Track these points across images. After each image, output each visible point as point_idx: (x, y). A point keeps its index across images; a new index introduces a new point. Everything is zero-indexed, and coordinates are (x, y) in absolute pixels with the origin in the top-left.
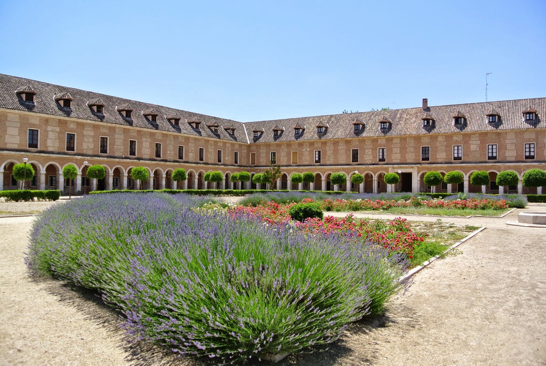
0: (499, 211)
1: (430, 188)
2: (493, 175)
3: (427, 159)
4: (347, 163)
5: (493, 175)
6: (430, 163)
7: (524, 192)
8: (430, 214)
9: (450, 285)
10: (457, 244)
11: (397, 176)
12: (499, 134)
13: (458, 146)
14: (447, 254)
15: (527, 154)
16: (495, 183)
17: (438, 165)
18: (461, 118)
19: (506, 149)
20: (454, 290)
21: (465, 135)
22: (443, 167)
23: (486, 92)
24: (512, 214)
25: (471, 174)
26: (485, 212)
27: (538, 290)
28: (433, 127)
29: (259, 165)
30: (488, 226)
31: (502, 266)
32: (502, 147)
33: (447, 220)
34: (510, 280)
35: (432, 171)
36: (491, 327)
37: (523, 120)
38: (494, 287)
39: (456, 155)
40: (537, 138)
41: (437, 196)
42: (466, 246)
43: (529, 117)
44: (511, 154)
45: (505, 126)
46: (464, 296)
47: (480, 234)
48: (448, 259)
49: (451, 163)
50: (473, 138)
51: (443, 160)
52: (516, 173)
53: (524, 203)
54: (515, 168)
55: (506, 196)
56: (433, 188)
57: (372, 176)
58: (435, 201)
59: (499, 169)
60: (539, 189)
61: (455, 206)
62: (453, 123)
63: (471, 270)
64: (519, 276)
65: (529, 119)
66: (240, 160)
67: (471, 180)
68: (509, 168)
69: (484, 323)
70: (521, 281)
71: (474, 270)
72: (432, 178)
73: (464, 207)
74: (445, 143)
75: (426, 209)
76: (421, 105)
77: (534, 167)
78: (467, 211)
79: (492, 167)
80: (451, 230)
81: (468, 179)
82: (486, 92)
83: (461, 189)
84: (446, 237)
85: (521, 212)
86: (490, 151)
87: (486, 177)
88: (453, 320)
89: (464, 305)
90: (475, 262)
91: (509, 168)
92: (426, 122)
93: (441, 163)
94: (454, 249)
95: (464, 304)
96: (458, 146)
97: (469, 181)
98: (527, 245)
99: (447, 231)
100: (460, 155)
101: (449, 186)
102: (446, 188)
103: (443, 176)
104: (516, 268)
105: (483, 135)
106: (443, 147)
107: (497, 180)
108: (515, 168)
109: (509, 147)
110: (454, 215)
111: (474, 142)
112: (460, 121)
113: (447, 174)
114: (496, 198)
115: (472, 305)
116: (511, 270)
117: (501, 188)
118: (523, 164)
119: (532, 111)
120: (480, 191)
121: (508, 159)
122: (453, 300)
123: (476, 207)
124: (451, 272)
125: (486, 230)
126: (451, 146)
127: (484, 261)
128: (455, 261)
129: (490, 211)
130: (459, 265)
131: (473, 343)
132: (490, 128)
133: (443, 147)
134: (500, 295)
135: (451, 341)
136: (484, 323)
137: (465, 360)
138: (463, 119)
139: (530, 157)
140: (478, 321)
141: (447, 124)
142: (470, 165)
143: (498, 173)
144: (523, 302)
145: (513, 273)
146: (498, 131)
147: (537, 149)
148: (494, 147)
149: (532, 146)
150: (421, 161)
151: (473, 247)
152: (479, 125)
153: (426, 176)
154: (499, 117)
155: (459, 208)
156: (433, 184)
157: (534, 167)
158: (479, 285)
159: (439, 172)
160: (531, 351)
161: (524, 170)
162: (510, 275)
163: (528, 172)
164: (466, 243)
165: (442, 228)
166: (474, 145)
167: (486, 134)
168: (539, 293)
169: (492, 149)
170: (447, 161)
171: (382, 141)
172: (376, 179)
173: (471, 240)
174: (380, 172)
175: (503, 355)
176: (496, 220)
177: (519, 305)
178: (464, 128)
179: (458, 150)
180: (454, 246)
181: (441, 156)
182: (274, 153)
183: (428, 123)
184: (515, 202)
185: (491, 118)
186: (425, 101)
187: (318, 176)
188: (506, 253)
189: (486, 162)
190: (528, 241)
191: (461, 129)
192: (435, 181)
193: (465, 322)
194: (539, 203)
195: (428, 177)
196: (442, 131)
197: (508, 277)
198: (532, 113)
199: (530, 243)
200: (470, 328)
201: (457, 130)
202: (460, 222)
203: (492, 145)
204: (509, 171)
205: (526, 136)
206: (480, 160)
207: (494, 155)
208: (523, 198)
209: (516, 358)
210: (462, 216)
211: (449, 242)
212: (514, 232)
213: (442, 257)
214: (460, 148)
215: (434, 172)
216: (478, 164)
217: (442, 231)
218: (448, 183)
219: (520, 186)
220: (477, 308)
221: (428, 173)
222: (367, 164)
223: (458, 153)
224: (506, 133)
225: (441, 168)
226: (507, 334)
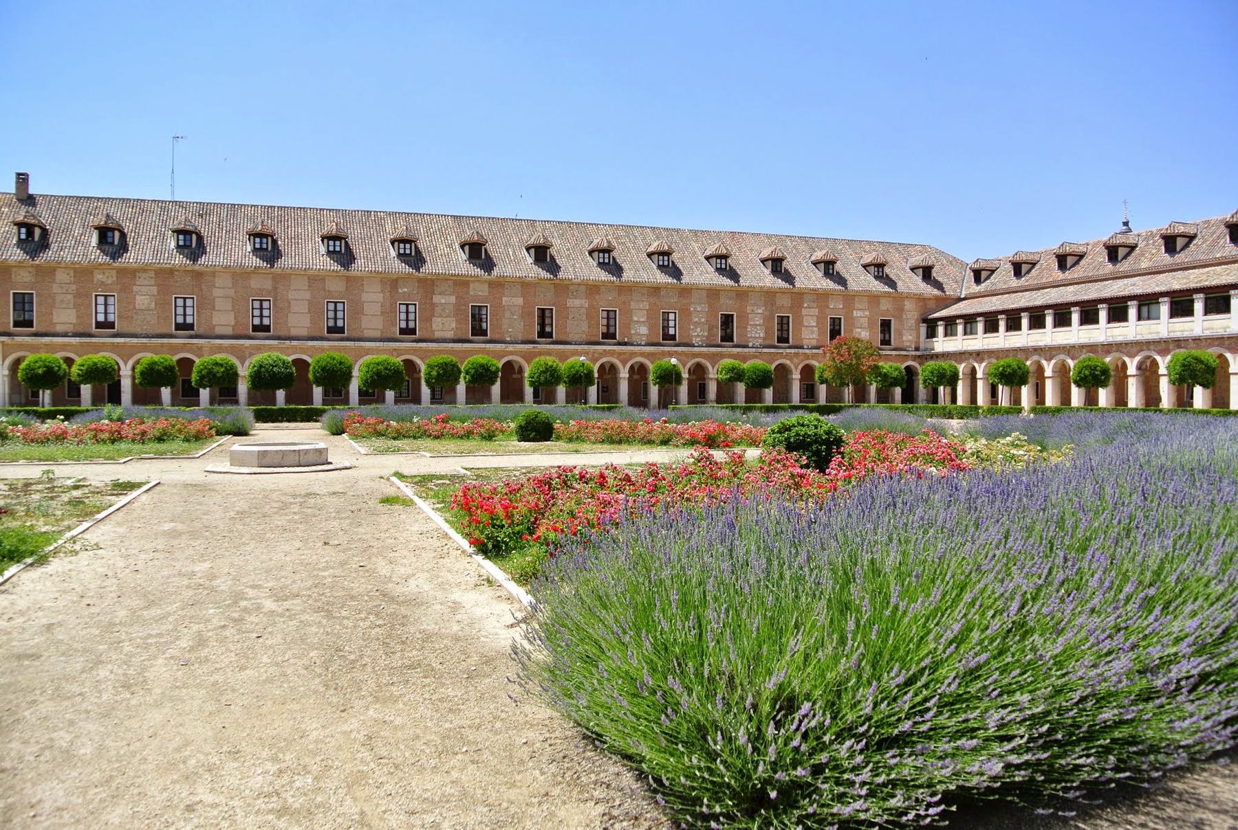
0: (193, 445)
1: (36, 395)
2: (186, 364)
4: (460, 336)
5: (186, 364)
6: (36, 335)
7: (252, 400)
8: (30, 459)
9: (49, 627)
10: (85, 525)
12: (198, 275)
13: (106, 296)
14: (56, 552)
15: (257, 321)
16: (189, 381)
17: (56, 339)
18: (113, 230)
19: (214, 309)
20: (60, 634)
21: (122, 272)
23: (172, 178)
24: (220, 449)
25: (138, 362)
26: (162, 447)
27: (243, 603)
28: (44, 244)
29: (52, 330)
30: (165, 478)
31: (178, 565)
32: (206, 304)
33: (67, 472)
34: (191, 593)
35: (271, 353)
36: (134, 702)
37: (249, 248)
38: (155, 612)
39: (101, 318)
40: (275, 288)
41: (52, 415)
42: (104, 528)
43: (261, 243)
44: (223, 320)
45: (210, 259)
46: (78, 646)
47: (144, 497)
48: (55, 565)
49: (90, 335)
50: (142, 279)
51: (69, 328)
52: (234, 361)
53: (247, 426)
54: (232, 350)
55: (212, 411)
56: (46, 396)
57: (521, 370)
58: (48, 426)
59: (199, 351)
60: (281, 394)
61: (95, 436)
62: (94, 240)
63: (108, 582)
64: (211, 580)
65: (261, 249)
67: (137, 375)
68: (220, 349)
69: (118, 698)
70: (213, 589)
71: (114, 580)
72: (40, 371)
73: (116, 438)
74: (74, 287)
75: (19, 448)
76: (11, 188)
77: (270, 348)
78: (123, 446)
79: (184, 347)
80: (76, 493)
81: (130, 373)
82: (172, 178)
83: (115, 398)
84: (59, 513)
85: (237, 445)
86: (180, 311)
87: (170, 369)
88: (46, 707)
89: (79, 666)
90: (121, 564)
91: (220, 349)
92: (23, 230)
93: (65, 335)
94: (73, 540)
95: (78, 663)
96: (106, 296)
97: (134, 378)
98: (238, 513)
99: (65, 498)
100: (111, 318)
101: (86, 390)
102: (79, 395)
103: (70, 366)
104: (207, 565)
105: (165, 275)
106: (70, 297)
107: (194, 377)
108: (232, 350)
109: (219, 304)
110: (90, 459)
111: (144, 289)
112: (192, 243)
113: (79, 360)
114: (188, 416)
115: (99, 662)
116: (197, 569)
117: (205, 394)
118: (247, 342)
119: (265, 231)
120: (157, 400)
121: (218, 331)
122: (53, 659)
123: (142, 438)
124: (57, 595)
125: (157, 488)
126: (88, 295)
127: (143, 556)
128: (70, 567)
129: (177, 445)
130: (82, 576)
131: (87, 750)
132: (179, 260)
133: (70, 297)
134: (164, 627)
135: (32, 758)
136: (118, 698)
137: (61, 793)
138: (117, 234)
139: (262, 328)
140: (105, 697)
141: (78, 242)
142: (135, 340)
143: (197, 361)
144: (210, 634)
145: (199, 575)
146: (197, 267)
147: (276, 312)
148: (189, 303)
149: (266, 304)
150: (12, 328)
151: (121, 530)
152: (156, 252)
153: (23, 365)
154: (200, 238)
155: (104, 441)
156: (45, 387)
157: (270, 348)
158: (122, 614)
159: (59, 355)
160: (210, 733)
161: (251, 355)
162: (196, 580)
163: (257, 358)
164: (107, 521)
165: (52, 489)
166: (145, 296)
167: (171, 272)
168: (245, 610)
169: (185, 307)
170: (80, 329)
171: (336, 286)
173: (120, 514)
174: (604, 360)
175: (150, 758)
176: (185, 463)
177: (201, 642)
178: (121, 256)
179: (106, 305)
180: (74, 532)
181: (65, 318)
183: (30, 233)
184: (228, 424)
185: (181, 237)
186: (22, 179)
187: (783, 370)
188: (193, 535)
189: (171, 336)
190: (242, 505)
191: (115, 256)
192: (48, 377)
193: (73, 705)
194: (285, 424)
195: (29, 368)
196: (67, 256)
197: (188, 587)
198: (266, 236)
199: (246, 507)
200: (84, 716)
201: (104, 259)
202: (99, 473)
204: (218, 357)
205: (255, 283)
206: (158, 331)
207: (189, 320)
208: (244, 412)
209: (177, 756)
210: (110, 458)
211: (66, 523)
212: (217, 488)
213: (42, 561)
214: (111, 300)
215: (44, 356)
216: (154, 340)
217: (52, 498)
218: (81, 382)
219: (243, 388)
220: (110, 666)
221: (30, 358)
223: (106, 313)
224: (214, 274)
225: (64, 347)
226: (165, 711)
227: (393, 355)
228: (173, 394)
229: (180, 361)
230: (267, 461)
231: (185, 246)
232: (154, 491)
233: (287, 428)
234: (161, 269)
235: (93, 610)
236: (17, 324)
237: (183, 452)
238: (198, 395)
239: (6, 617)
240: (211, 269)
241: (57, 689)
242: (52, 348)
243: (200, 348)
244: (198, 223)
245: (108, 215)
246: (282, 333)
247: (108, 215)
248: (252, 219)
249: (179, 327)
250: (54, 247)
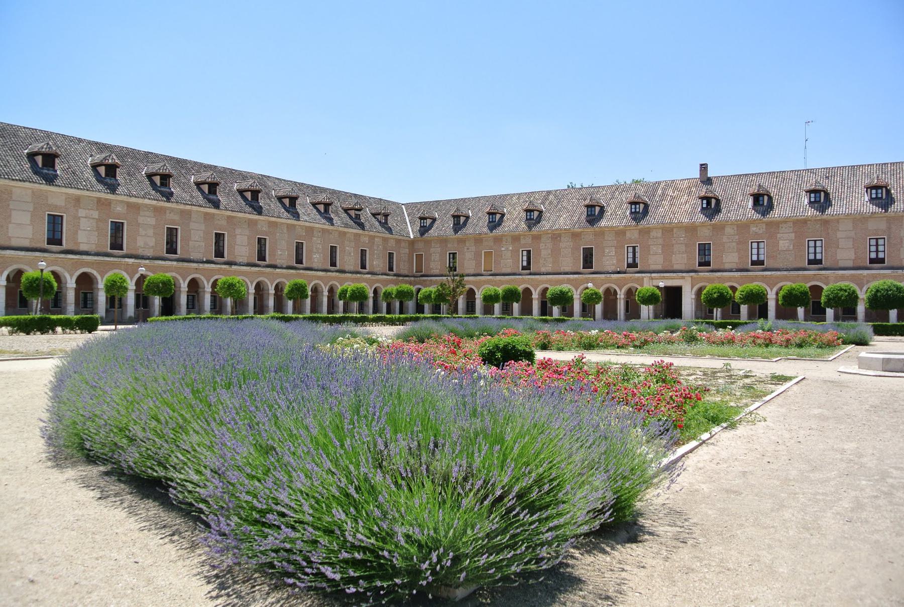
0: (826, 351)
1: (711, 312)
2: (817, 290)
3: (708, 264)
4: (575, 270)
5: (817, 290)
6: (712, 271)
7: (868, 318)
8: (713, 355)
10: (757, 404)
12: (826, 222)
14: (740, 421)
15: (873, 255)
16: (820, 303)
17: (725, 274)
18: (763, 195)
21: (770, 224)
22: (734, 277)
23: (805, 154)
25: (781, 289)
26: (803, 351)
27: (890, 481)
28: (718, 210)
29: (722, 267)
33: (740, 366)
34: (844, 465)
35: (714, 283)
36: (813, 542)
37: (867, 198)
40: (889, 228)
41: (723, 326)
42: (770, 407)
43: (877, 193)
44: (846, 255)
45: (836, 209)
47: (795, 388)
48: (741, 430)
49: (747, 270)
52: (854, 287)
53: (867, 337)
54: (852, 279)
55: (839, 325)
56: (717, 312)
57: (615, 292)
58: (721, 333)
60: (893, 314)
61: (754, 341)
62: (750, 203)
64: (860, 458)
65: (877, 198)
67: (780, 298)
68: (843, 278)
69: (801, 536)
70: (862, 466)
71: (784, 447)
72: (715, 296)
73: (769, 343)
75: (705, 347)
76: (697, 175)
77: (884, 276)
78: (774, 349)
79: (814, 277)
80: (747, 381)
81: (774, 296)
82: (805, 154)
83: (763, 314)
84: (738, 394)
85: (863, 352)
86: (812, 250)
87: (804, 293)
90: (787, 435)
91: (843, 278)
92: (705, 202)
93: (731, 271)
94: (751, 413)
97: (777, 300)
98: (872, 406)
99: (740, 383)
100: (762, 258)
101: (744, 309)
102: (739, 312)
104: (853, 445)
105: (800, 224)
107: (823, 299)
109: (842, 243)
110: (752, 357)
112: (820, 198)
113: (740, 288)
115: (782, 506)
116: (846, 447)
117: (830, 312)
118: (866, 272)
119: (880, 184)
120: (794, 316)
121: (841, 264)
123: (787, 344)
125: (804, 381)
128: (752, 433)
129: (812, 350)
132: (811, 212)
133: (734, 244)
135: (746, 566)
138: (766, 198)
140: (791, 533)
141: (739, 206)
142: (779, 273)
143: (825, 287)
146: (825, 217)
148: (818, 243)
149: (881, 242)
150: (697, 268)
151: (783, 410)
152: (794, 208)
153: (705, 292)
154: (827, 194)
155: (760, 345)
156: (717, 306)
157: (884, 276)
158: (794, 473)
159: (727, 285)
161: (868, 282)
163: (874, 285)
165: (731, 377)
166: (785, 241)
167: (805, 221)
168: (892, 486)
169: (815, 247)
170: (741, 267)
172: (622, 296)
173: (779, 398)
176: (821, 364)
177: (859, 506)
178: (768, 213)
179: (758, 248)
180: (752, 408)
181: (731, 259)
183: (709, 203)
184: (852, 335)
185: (813, 195)
186: (704, 167)
187: (527, 292)
191: (764, 214)
193: (769, 535)
194: (893, 337)
195: (709, 294)
196: (732, 216)
197: (842, 460)
198: (881, 187)
202: (762, 368)
204: (843, 284)
205: (872, 225)
206: (795, 266)
207: (819, 257)
208: (866, 328)
210: (766, 358)
211: (744, 401)
212: (850, 385)
213: (732, 426)
214: (761, 245)
215: (718, 285)
217: (732, 383)
218: (742, 303)
219: (861, 309)
220: (790, 510)
223: (758, 254)
224: (838, 221)
225: (730, 279)
227: (801, 282)
228: (806, 312)
229: (811, 288)
230: (890, 366)
231: (815, 202)
232: (801, 383)
233: (901, 341)
234: (798, 220)
235: (772, 466)
236: (700, 264)
237: (819, 355)
238: (824, 313)
239: (715, 462)
240: (836, 217)
241: (756, 519)
242: (721, 280)
243: (827, 278)
244: (886, 179)
245: (759, 185)
246: (895, 264)
247: (759, 185)
248: (869, 175)
249: (810, 262)
250: (724, 211)
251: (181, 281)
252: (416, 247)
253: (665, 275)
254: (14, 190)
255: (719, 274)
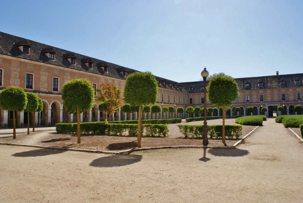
3: (285, 99)
4: (244, 102)
6: (286, 101)
11: (283, 107)
22: (293, 103)
57: (243, 109)
66: (171, 100)
93: (292, 101)
133: (292, 94)
150: (281, 100)
172: (259, 109)
182: (299, 94)
187: (242, 108)
203: (247, 96)
207: (248, 100)
222: (254, 103)
236: (282, 100)
251: (287, 107)
252: (190, 96)
253: (272, 103)
254: (122, 82)
255: (288, 102)
